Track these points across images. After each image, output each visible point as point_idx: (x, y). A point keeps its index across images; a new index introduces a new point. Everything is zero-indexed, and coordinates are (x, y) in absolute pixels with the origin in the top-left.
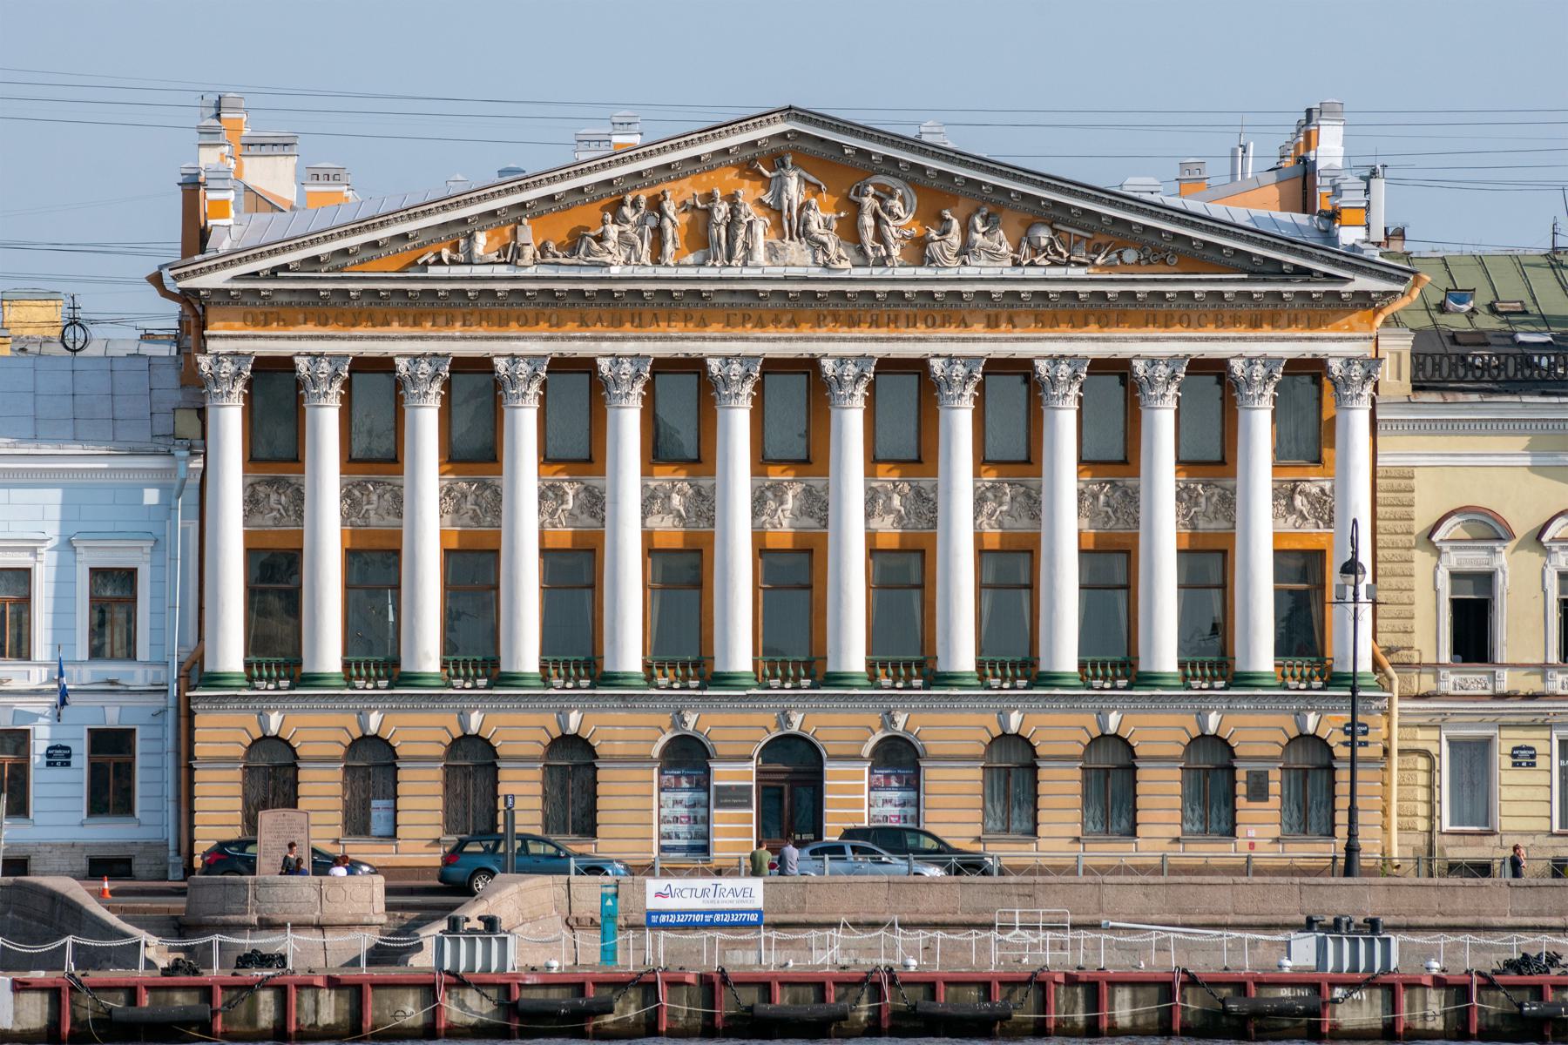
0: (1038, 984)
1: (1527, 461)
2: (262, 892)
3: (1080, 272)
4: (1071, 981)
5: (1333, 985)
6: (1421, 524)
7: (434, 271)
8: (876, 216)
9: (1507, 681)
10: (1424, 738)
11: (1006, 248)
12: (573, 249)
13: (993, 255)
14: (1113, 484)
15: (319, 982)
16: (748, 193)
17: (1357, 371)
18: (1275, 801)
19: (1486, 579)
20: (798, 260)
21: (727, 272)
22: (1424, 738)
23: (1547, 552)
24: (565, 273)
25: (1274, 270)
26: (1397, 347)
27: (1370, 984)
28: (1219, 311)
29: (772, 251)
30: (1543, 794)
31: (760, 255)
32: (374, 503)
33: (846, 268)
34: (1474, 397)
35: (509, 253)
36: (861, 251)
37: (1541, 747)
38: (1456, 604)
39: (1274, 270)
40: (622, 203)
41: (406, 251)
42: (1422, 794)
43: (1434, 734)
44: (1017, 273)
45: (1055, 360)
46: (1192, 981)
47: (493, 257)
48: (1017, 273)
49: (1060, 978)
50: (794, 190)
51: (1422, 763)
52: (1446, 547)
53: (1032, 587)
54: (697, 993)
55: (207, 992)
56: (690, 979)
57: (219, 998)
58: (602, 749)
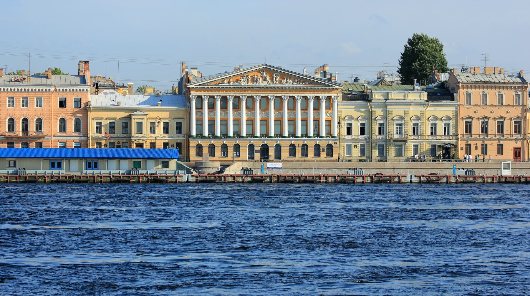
0: (320, 177)
1: (354, 109)
2: (205, 163)
3: (301, 85)
4: (324, 176)
5: (356, 177)
6: (343, 117)
7: (219, 85)
8: (275, 78)
9: (438, 137)
10: (343, 144)
11: (292, 82)
12: (237, 82)
13: (290, 83)
14: (279, 112)
15: (229, 176)
16: (259, 75)
17: (336, 98)
18: (325, 152)
19: (351, 124)
20: (265, 83)
21: (256, 85)
22: (343, 144)
23: (358, 121)
24: (236, 85)
25: (322, 84)
26: (340, 95)
27: (361, 176)
28: (318, 90)
29: (262, 82)
30: (358, 151)
31: (261, 83)
32: (316, 114)
33: (272, 84)
34: (350, 101)
35: (229, 83)
36: (274, 82)
37: (358, 145)
38: (347, 127)
39: (322, 84)
40: (243, 76)
41: (216, 82)
42: (343, 151)
43: (344, 144)
44: (293, 85)
45: (298, 96)
46: (339, 176)
47: (227, 83)
48: (293, 85)
49: (322, 176)
50: (265, 75)
51: (343, 147)
52: (346, 120)
53: (202, 125)
54: (276, 177)
55: (215, 177)
56: (276, 176)
57: (217, 178)
58: (269, 145)
